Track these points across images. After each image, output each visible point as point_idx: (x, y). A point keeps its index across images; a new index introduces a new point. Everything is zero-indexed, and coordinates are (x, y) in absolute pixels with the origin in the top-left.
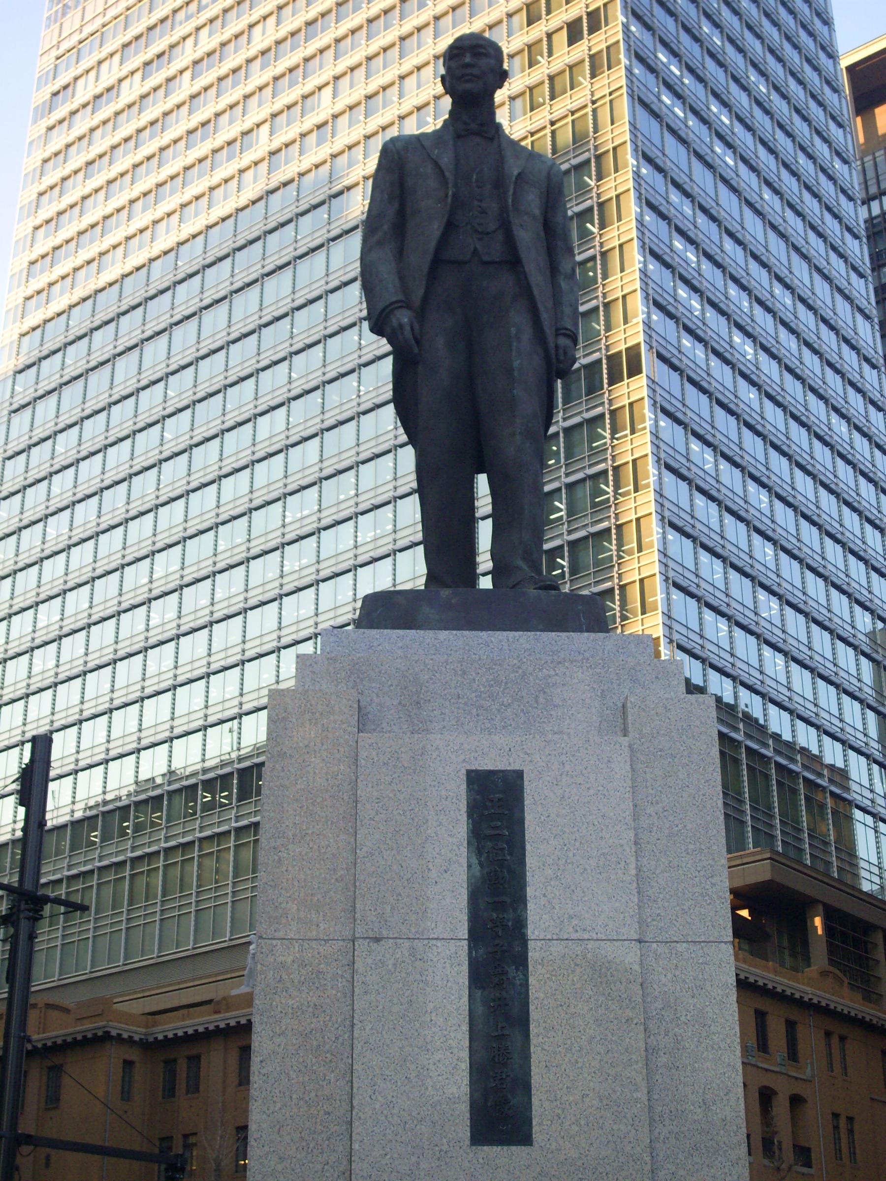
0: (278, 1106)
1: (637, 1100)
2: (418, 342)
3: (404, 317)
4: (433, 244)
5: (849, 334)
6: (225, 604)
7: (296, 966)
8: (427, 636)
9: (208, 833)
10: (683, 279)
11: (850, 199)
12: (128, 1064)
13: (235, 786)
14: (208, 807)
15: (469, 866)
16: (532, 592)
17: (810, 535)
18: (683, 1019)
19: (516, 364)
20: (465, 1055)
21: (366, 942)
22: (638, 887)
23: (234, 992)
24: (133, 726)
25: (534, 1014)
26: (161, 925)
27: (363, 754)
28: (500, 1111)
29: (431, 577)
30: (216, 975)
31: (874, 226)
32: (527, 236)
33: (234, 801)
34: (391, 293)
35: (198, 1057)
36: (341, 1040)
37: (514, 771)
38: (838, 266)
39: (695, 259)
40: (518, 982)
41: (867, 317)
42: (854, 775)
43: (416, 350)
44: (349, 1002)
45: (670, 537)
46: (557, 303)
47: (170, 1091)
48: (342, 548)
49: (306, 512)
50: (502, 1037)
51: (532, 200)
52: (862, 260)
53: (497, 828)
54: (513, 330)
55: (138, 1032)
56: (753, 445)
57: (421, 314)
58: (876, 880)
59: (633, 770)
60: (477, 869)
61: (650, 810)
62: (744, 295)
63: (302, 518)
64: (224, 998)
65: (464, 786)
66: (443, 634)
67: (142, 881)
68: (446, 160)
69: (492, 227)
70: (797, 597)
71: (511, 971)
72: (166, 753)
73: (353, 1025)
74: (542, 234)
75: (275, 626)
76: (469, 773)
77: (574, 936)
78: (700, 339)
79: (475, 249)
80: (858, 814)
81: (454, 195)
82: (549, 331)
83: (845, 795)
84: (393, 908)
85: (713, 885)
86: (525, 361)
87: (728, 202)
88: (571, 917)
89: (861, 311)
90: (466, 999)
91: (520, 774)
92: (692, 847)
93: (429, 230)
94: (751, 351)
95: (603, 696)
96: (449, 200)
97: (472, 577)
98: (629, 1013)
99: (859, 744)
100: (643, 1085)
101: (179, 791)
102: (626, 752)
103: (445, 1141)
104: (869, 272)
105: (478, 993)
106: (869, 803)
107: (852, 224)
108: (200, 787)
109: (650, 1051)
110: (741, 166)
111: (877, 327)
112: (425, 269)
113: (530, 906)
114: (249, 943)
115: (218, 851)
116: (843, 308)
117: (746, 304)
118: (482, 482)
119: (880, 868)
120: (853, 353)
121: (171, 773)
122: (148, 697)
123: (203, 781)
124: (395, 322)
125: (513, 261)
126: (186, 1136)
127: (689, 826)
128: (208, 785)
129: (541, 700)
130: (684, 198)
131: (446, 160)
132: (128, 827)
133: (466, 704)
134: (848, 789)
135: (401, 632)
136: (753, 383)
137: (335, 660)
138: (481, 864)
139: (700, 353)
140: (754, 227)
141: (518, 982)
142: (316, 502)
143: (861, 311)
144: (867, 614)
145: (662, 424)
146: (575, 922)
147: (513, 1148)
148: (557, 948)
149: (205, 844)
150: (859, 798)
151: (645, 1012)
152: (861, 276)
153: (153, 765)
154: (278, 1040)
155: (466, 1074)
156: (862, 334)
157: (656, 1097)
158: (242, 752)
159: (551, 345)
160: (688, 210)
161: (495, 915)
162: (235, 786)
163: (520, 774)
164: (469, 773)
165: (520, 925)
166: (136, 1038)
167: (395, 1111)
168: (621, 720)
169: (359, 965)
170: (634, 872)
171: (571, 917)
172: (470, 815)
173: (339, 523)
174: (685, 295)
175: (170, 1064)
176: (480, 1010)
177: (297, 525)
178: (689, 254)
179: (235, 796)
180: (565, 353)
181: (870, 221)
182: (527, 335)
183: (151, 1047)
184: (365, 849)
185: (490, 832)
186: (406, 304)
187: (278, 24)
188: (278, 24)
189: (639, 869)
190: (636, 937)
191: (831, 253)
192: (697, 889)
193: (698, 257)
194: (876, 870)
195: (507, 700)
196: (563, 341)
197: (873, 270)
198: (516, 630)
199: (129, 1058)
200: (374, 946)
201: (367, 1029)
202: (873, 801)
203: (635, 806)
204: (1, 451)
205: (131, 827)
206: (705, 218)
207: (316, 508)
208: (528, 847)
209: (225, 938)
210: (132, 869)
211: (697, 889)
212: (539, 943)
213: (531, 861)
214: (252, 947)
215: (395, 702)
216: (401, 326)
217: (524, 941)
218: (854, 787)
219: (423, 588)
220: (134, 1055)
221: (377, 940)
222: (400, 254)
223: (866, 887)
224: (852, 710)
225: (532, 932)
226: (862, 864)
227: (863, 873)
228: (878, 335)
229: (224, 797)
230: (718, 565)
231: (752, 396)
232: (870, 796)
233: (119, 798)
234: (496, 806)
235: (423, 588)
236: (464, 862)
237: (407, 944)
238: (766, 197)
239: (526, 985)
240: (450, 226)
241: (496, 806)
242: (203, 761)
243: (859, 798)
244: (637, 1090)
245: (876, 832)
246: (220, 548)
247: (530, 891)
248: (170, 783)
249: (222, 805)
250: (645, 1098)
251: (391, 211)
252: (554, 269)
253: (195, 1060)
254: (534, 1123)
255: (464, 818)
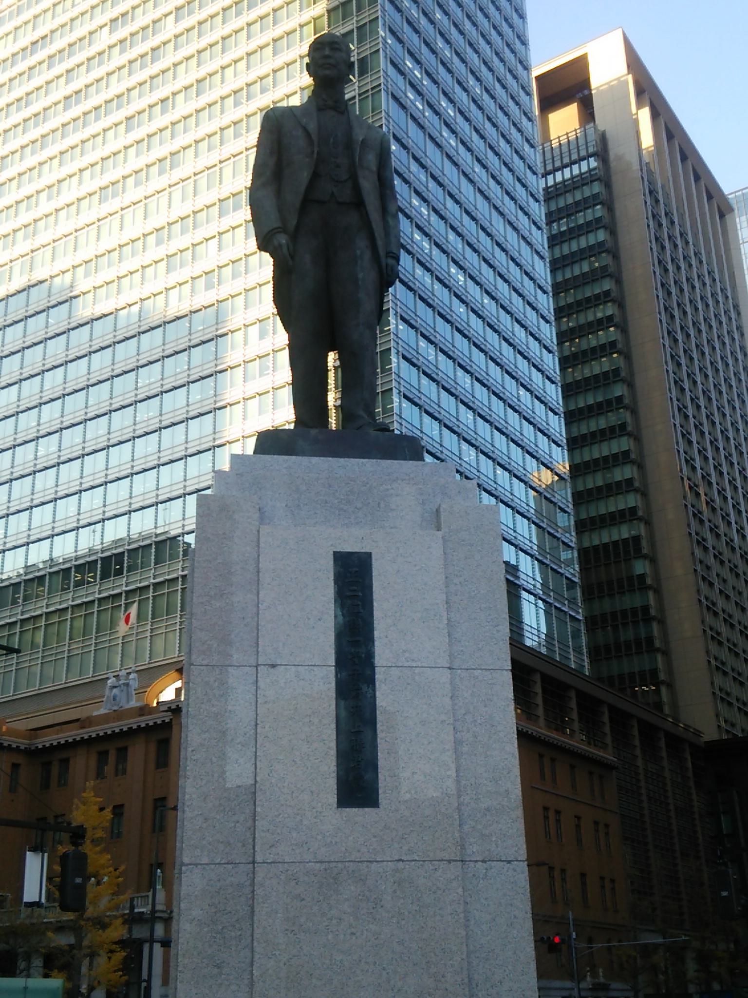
0: (204, 782)
1: (449, 777)
2: (292, 257)
3: (283, 239)
4: (303, 188)
5: (529, 269)
6: (93, 442)
7: (217, 684)
8: (304, 461)
9: (78, 602)
10: (418, 227)
11: (534, 173)
12: (15, 766)
13: (99, 569)
14: (78, 584)
15: (336, 617)
16: (373, 433)
17: (497, 406)
18: (479, 721)
19: (361, 275)
20: (333, 745)
21: (265, 668)
22: (449, 632)
23: (95, 713)
24: (24, 526)
25: (379, 717)
26: (42, 667)
27: (262, 540)
28: (358, 784)
29: (297, 422)
30: (81, 702)
31: (549, 193)
32: (368, 185)
33: (98, 579)
34: (273, 222)
35: (125, 749)
36: (248, 735)
37: (365, 553)
38: (523, 222)
39: (426, 213)
40: (369, 696)
41: (542, 258)
42: (522, 568)
43: (291, 263)
44: (254, 708)
45: (404, 405)
46: (387, 234)
47: (46, 785)
48: (178, 406)
49: (152, 380)
50: (358, 733)
51: (371, 159)
52: (540, 217)
53: (355, 590)
54: (358, 252)
55: (23, 743)
56: (461, 343)
57: (294, 237)
58: (536, 639)
59: (445, 553)
60: (341, 618)
61: (456, 581)
62: (459, 239)
63: (149, 384)
64: (88, 718)
65: (332, 562)
66: (315, 460)
67: (28, 636)
68: (312, 127)
69: (344, 177)
70: (488, 448)
71: (364, 688)
72: (49, 546)
73: (256, 725)
74: (377, 184)
75: (130, 459)
76: (335, 553)
77: (406, 664)
78: (428, 270)
79: (333, 193)
80: (524, 594)
81: (318, 153)
82: (382, 253)
83: (516, 581)
84: (284, 644)
85: (498, 631)
86: (367, 275)
87: (450, 172)
88: (404, 651)
89: (538, 253)
90: (334, 706)
91: (369, 555)
92: (484, 606)
93: (301, 176)
94: (462, 279)
95: (423, 504)
96: (315, 156)
97: (326, 423)
98: (443, 717)
99: (526, 548)
100: (453, 766)
101: (57, 572)
102: (441, 541)
103: (320, 804)
104: (544, 226)
105: (342, 703)
106: (532, 587)
107: (534, 191)
108: (73, 570)
109: (458, 743)
110: (461, 147)
111: (548, 265)
112: (298, 205)
113: (377, 643)
114: (108, 679)
115: (85, 615)
116: (526, 250)
117: (461, 246)
118: (332, 358)
119: (539, 631)
120: (506, 285)
121: (52, 560)
122: (36, 507)
123: (76, 566)
124: (276, 243)
125: (359, 203)
126: (56, 817)
127: (482, 592)
128: (78, 568)
129: (382, 505)
130: (421, 169)
131: (312, 127)
132: (19, 598)
133: (331, 507)
134: (518, 578)
135: (286, 457)
136: (463, 301)
137: (241, 475)
138: (343, 615)
139: (428, 279)
140: (467, 191)
141: (369, 696)
142: (160, 373)
143: (538, 253)
144: (534, 460)
145: (401, 327)
146: (407, 655)
147: (366, 809)
148: (395, 672)
149: (76, 610)
150: (525, 583)
151: (454, 716)
152: (539, 228)
153: (38, 555)
154: (204, 736)
155: (334, 758)
156: (537, 269)
157: (462, 774)
158: (79, 553)
159: (384, 264)
160: (423, 177)
161: (353, 650)
162: (99, 569)
163: (369, 555)
164: (335, 553)
165: (370, 656)
166: (22, 747)
167: (286, 784)
168: (436, 520)
169: (261, 684)
170: (446, 622)
171: (404, 651)
172: (336, 581)
173: (176, 388)
174: (419, 238)
175: (47, 765)
176: (343, 714)
177: (146, 389)
178: (422, 209)
179: (98, 576)
180: (392, 270)
181: (546, 189)
182: (368, 255)
183: (32, 753)
184: (265, 604)
185: (348, 594)
186: (283, 230)
187: (15, 41)
188: (15, 41)
189: (449, 620)
190: (448, 665)
191: (519, 212)
192: (487, 634)
193: (428, 211)
194: (536, 632)
195: (359, 505)
196: (391, 262)
197: (547, 224)
198: (363, 458)
199: (16, 761)
200: (272, 670)
201: (267, 727)
202: (534, 586)
203: (446, 577)
204: (2, 320)
205: (21, 598)
206: (435, 184)
207: (160, 377)
208: (375, 604)
209: (89, 676)
210: (21, 627)
211: (487, 634)
212: (383, 669)
213: (377, 614)
214: (109, 682)
215: (284, 505)
216: (280, 245)
217: (373, 667)
218: (522, 576)
219: (292, 426)
220: (19, 759)
221: (273, 666)
222: (279, 194)
223: (528, 643)
224: (523, 526)
225: (378, 661)
226: (526, 627)
227: (527, 634)
228: (548, 270)
229: (90, 577)
230: (436, 425)
231: (461, 310)
232: (533, 582)
233: (10, 578)
234: (353, 578)
235: (292, 426)
236: (332, 613)
237: (293, 669)
238: (477, 170)
239: (374, 697)
240: (315, 176)
241: (353, 578)
242: (76, 551)
243: (525, 583)
244: (449, 770)
245: (537, 606)
246: (90, 403)
247: (376, 634)
248: (51, 567)
249: (89, 582)
250: (454, 775)
251: (272, 162)
252: (384, 210)
253: (65, 762)
254: (380, 792)
255: (331, 583)
